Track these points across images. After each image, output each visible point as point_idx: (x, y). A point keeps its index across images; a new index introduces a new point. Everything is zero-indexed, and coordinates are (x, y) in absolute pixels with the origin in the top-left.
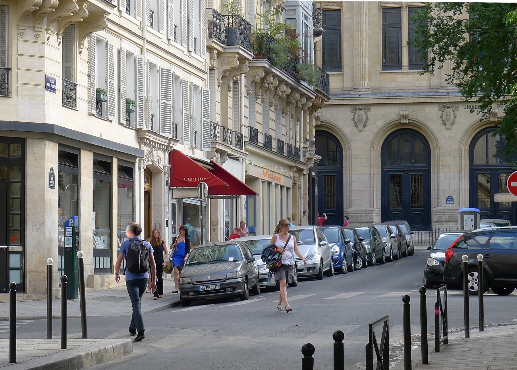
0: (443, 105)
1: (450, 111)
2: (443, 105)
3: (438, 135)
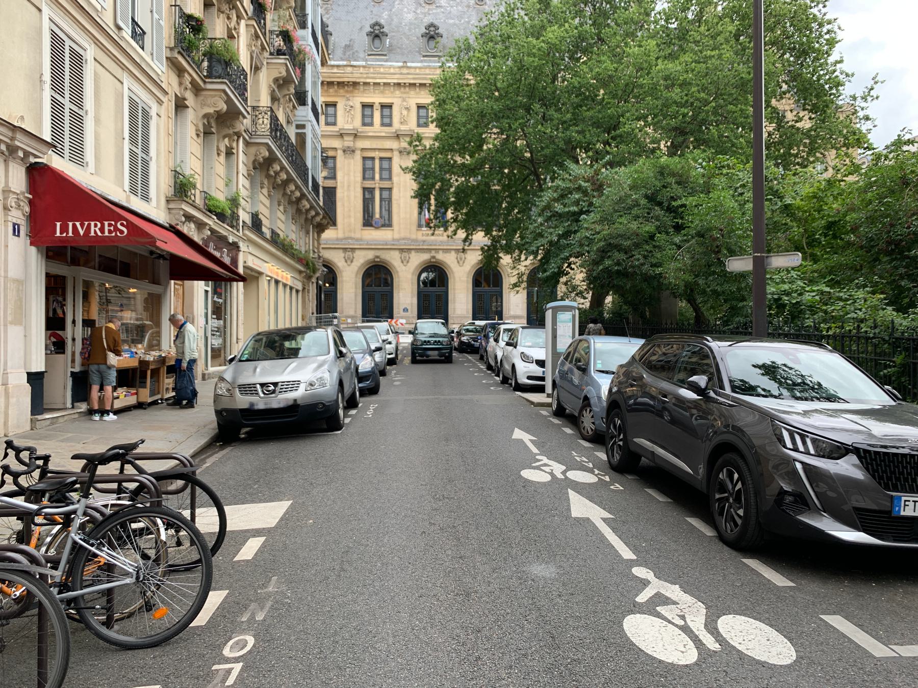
0: (401, 250)
1: (406, 254)
2: (401, 250)
3: (398, 269)
